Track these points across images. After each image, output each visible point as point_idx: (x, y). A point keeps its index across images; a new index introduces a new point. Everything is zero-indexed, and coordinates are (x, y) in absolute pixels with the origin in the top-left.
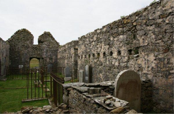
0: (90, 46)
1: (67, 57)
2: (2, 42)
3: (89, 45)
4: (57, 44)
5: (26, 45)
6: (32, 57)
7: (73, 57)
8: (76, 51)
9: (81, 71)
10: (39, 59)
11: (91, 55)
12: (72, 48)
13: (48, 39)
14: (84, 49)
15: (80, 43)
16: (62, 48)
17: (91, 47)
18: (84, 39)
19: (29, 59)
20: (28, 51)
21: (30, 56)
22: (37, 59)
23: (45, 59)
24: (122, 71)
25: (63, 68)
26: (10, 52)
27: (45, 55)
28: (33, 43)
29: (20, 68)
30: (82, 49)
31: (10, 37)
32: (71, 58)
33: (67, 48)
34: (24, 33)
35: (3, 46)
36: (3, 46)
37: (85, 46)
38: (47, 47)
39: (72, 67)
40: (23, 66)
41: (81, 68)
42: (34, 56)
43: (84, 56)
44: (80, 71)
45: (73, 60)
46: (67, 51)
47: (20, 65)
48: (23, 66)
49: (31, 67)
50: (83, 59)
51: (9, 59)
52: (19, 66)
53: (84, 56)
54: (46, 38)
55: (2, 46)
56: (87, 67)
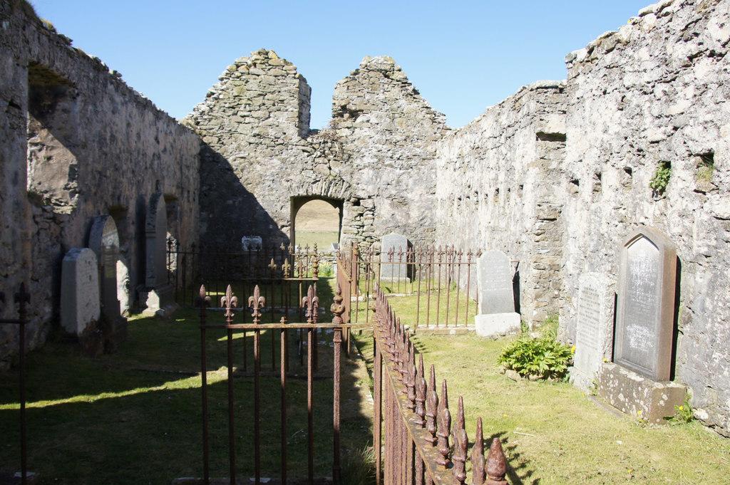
0: (669, 98)
1: (492, 192)
2: (150, 116)
3: (660, 88)
4: (433, 121)
5: (272, 132)
6: (302, 192)
7: (527, 187)
8: (548, 151)
9: (599, 282)
10: (337, 203)
11: (677, 165)
12: (526, 131)
13: (382, 97)
14: (614, 128)
15: (579, 94)
16: (458, 142)
17: (681, 105)
18: (609, 58)
19: (289, 205)
20: (283, 161)
21: (290, 188)
22: (329, 207)
23: (369, 204)
24: (200, 194)
25: (465, 258)
26: (201, 170)
27: (367, 183)
28: (308, 123)
29: (245, 248)
30: (600, 128)
31: (59, 32)
32: (513, 195)
33: (487, 134)
34: (261, 72)
35: (157, 139)
36: (157, 139)
37: (622, 105)
38: (377, 137)
39: (524, 248)
40: (259, 240)
41: (588, 259)
42: (316, 190)
43: (611, 177)
44: (584, 281)
45: (529, 210)
46: (491, 154)
47: (248, 235)
48: (259, 240)
49: (300, 248)
50: (607, 192)
51: (195, 206)
52: (244, 239)
53: (611, 177)
54: (373, 88)
55: (152, 140)
56: (644, 257)
